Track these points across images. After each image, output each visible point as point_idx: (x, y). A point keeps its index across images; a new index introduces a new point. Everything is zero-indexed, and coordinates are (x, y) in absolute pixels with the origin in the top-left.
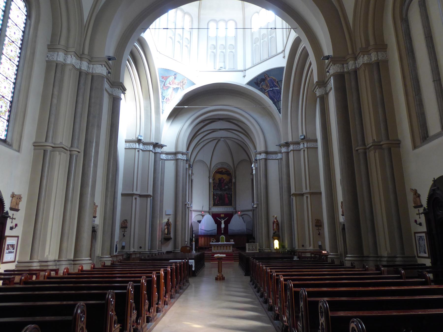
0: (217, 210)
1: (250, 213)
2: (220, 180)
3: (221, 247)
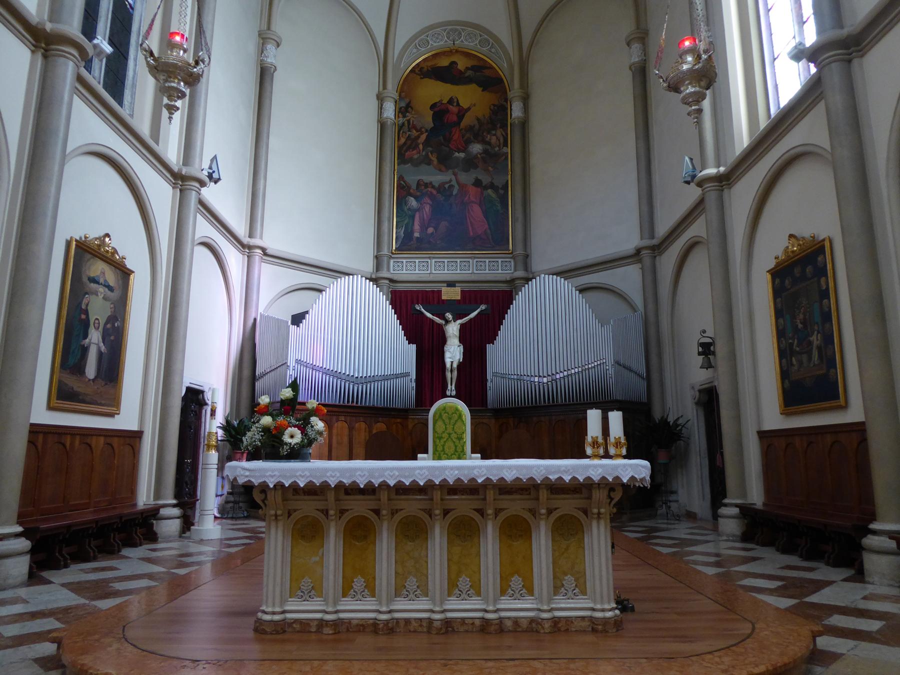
0: (415, 270)
1: (628, 279)
2: (439, 111)
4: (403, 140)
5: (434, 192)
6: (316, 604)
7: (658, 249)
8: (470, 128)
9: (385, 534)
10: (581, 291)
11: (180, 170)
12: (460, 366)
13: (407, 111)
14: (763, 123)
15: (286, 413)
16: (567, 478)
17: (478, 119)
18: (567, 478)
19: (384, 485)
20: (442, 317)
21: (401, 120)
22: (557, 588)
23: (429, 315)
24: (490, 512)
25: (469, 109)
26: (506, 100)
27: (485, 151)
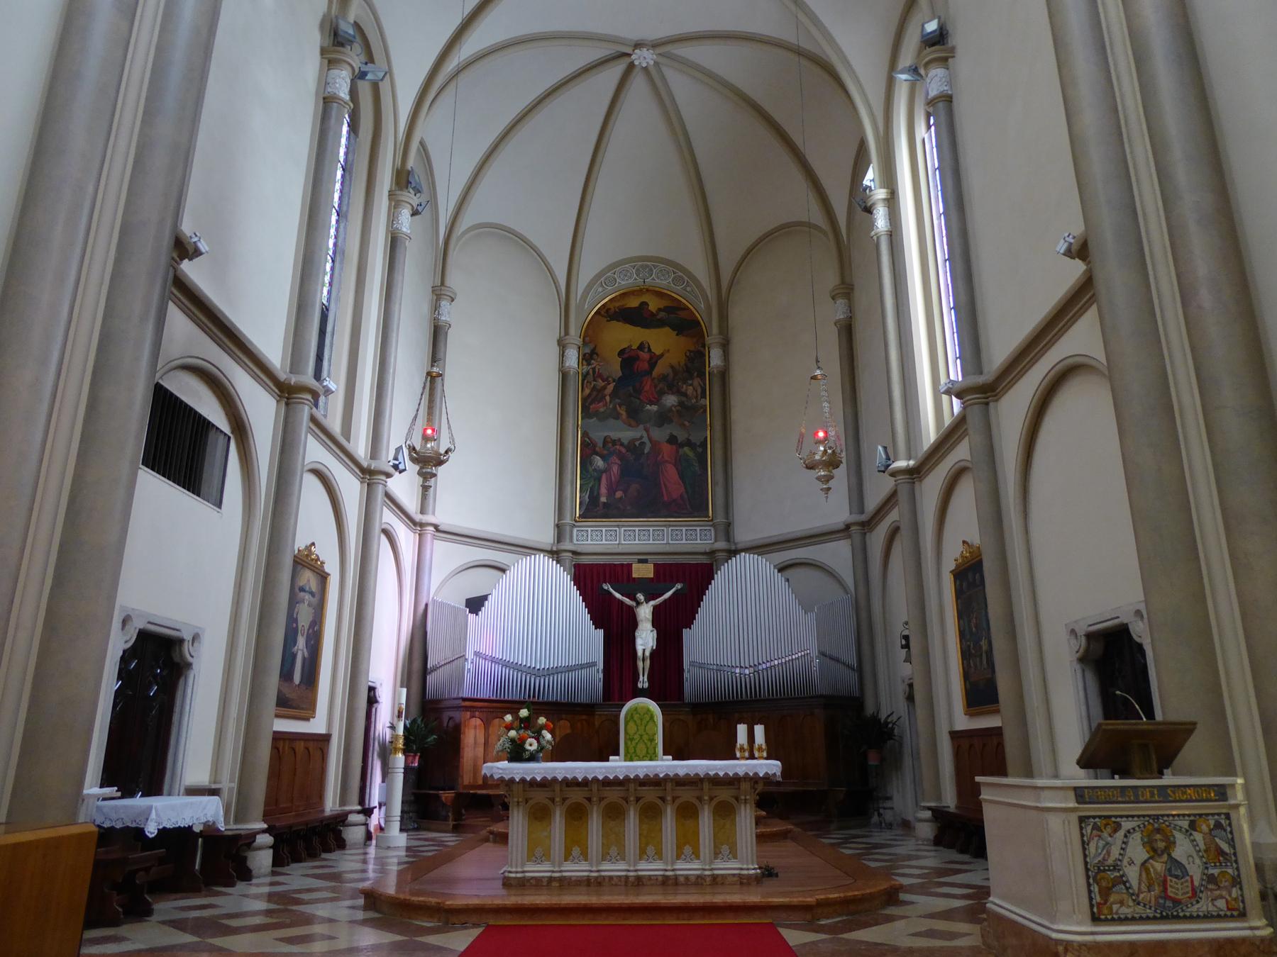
0: (604, 540)
1: (838, 555)
2: (628, 358)
3: (614, 813)
4: (587, 391)
5: (624, 450)
6: (546, 867)
7: (868, 525)
8: (663, 378)
9: (595, 816)
10: (781, 569)
11: (369, 465)
12: (653, 653)
13: (592, 358)
14: (948, 421)
15: (526, 728)
16: (721, 774)
17: (672, 367)
18: (721, 774)
19: (595, 779)
20: (633, 598)
21: (586, 368)
22: (716, 854)
23: (618, 595)
24: (669, 798)
25: (662, 355)
26: (704, 346)
27: (681, 404)
